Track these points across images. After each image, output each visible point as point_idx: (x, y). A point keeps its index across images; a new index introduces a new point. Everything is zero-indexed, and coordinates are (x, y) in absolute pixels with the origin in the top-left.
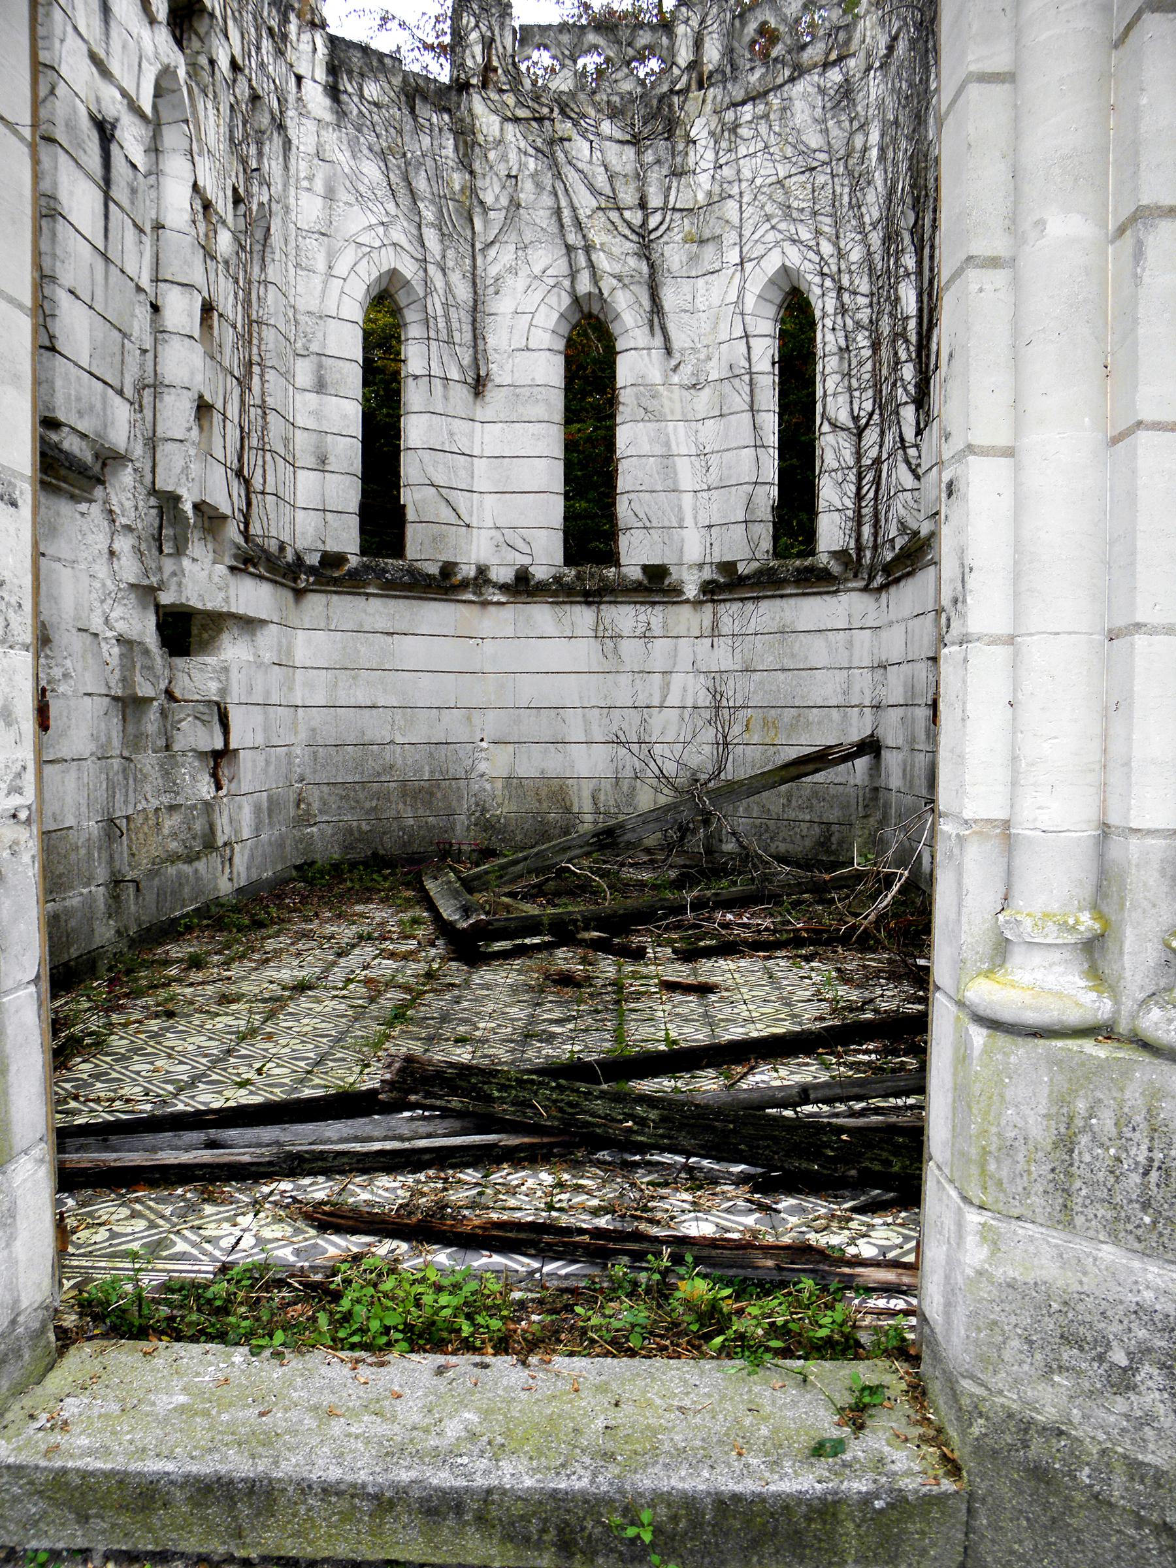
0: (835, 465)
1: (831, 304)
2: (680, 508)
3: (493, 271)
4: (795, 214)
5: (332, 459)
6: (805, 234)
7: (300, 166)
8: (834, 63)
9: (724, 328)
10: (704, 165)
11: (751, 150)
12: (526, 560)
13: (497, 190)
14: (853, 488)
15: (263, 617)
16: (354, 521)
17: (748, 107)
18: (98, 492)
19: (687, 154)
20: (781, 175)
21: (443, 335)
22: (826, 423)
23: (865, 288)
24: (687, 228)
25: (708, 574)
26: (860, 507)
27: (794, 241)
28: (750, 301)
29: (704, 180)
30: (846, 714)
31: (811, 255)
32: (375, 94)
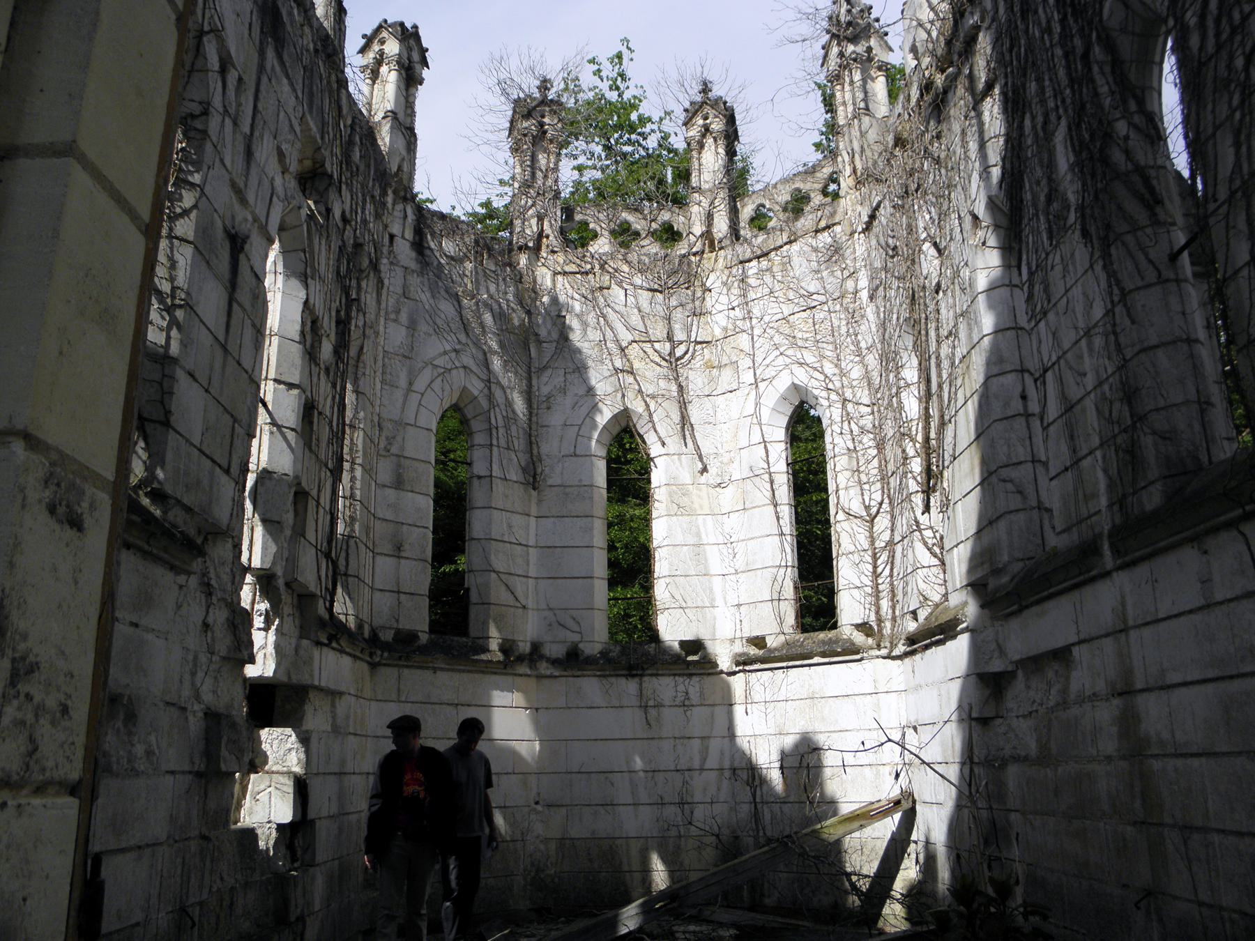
0: (852, 548)
1: (836, 412)
2: (711, 590)
3: (545, 390)
4: (800, 343)
5: (406, 546)
6: (810, 358)
7: (390, 301)
8: (824, 229)
9: (743, 435)
10: (719, 307)
11: (759, 295)
12: (576, 638)
13: (549, 326)
14: (870, 568)
15: (343, 689)
16: (426, 602)
17: (754, 263)
18: (197, 565)
19: (704, 299)
20: (786, 313)
21: (503, 442)
22: (840, 512)
23: (866, 400)
24: (707, 357)
25: (739, 648)
26: (878, 584)
27: (801, 364)
28: (765, 413)
29: (721, 319)
30: (878, 773)
31: (816, 375)
32: (452, 250)
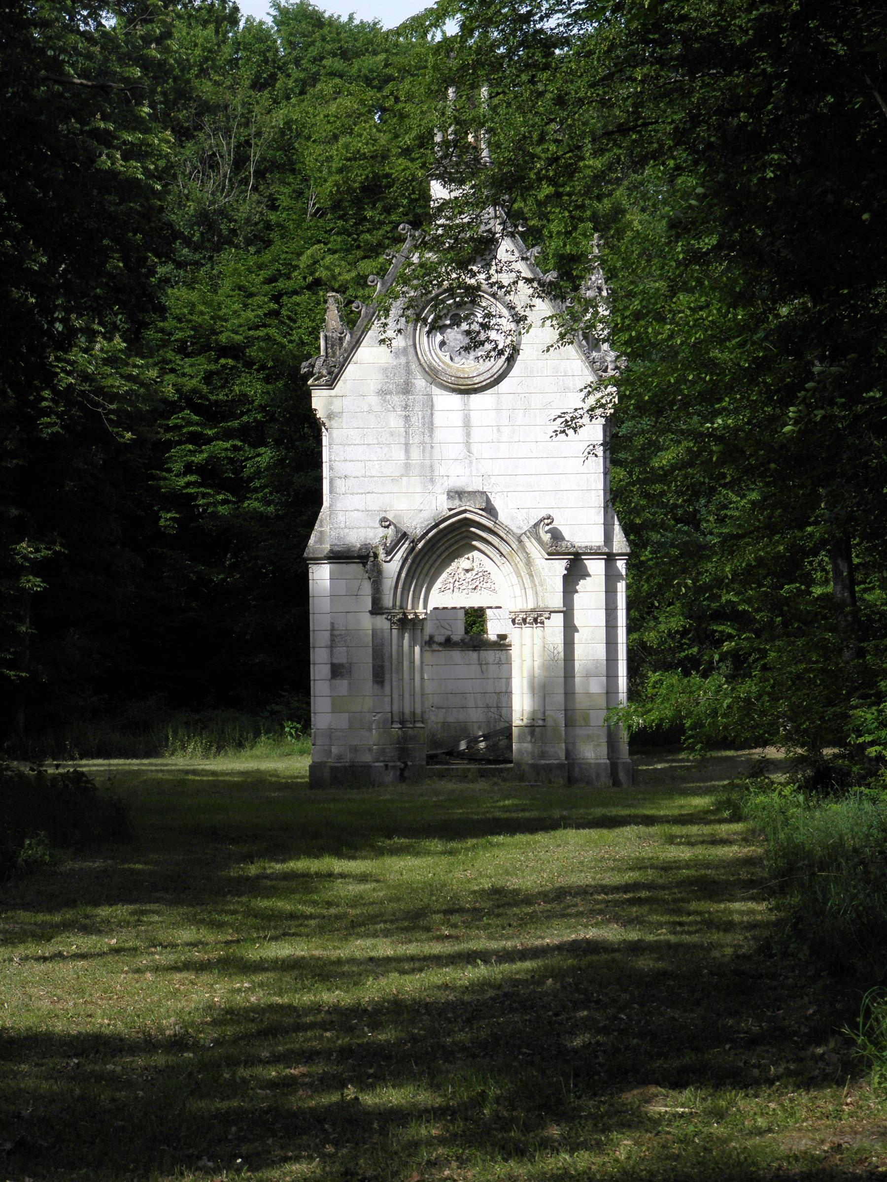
12: (449, 633)
